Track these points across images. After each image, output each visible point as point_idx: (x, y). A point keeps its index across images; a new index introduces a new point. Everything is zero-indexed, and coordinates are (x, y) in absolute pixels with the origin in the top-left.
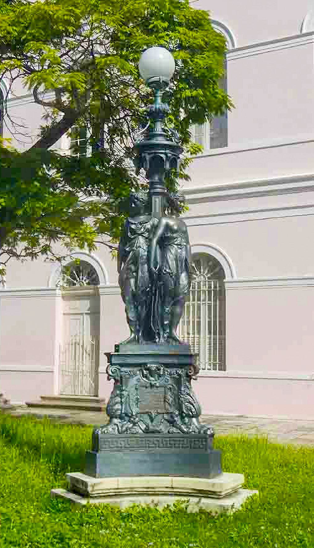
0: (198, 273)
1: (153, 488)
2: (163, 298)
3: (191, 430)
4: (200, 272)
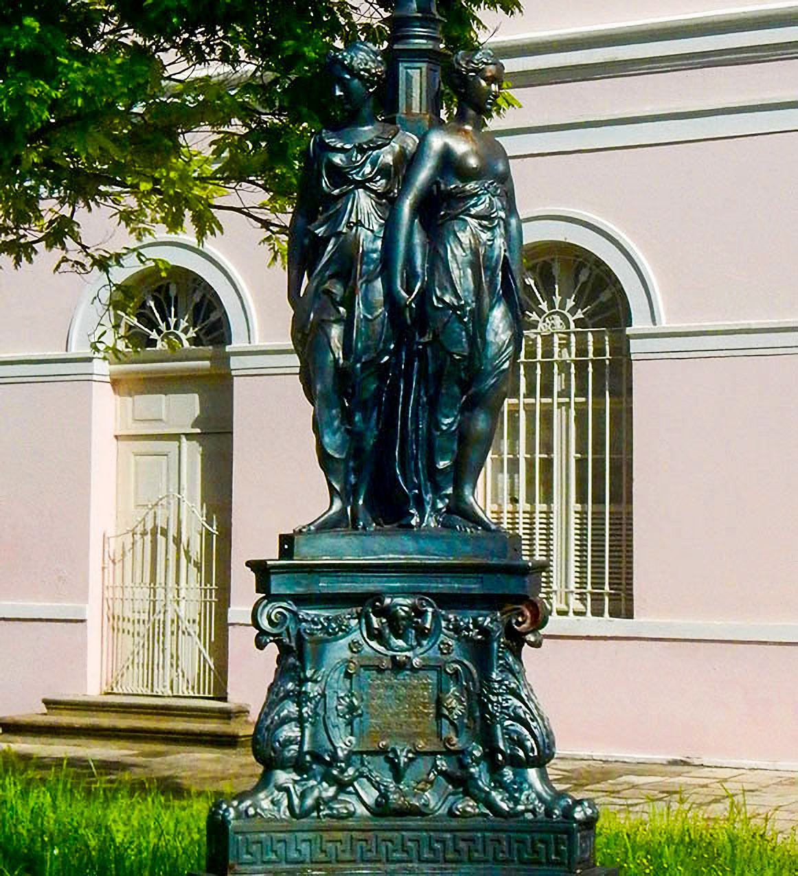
0: (544, 306)
2: (434, 383)
3: (521, 808)
4: (551, 305)
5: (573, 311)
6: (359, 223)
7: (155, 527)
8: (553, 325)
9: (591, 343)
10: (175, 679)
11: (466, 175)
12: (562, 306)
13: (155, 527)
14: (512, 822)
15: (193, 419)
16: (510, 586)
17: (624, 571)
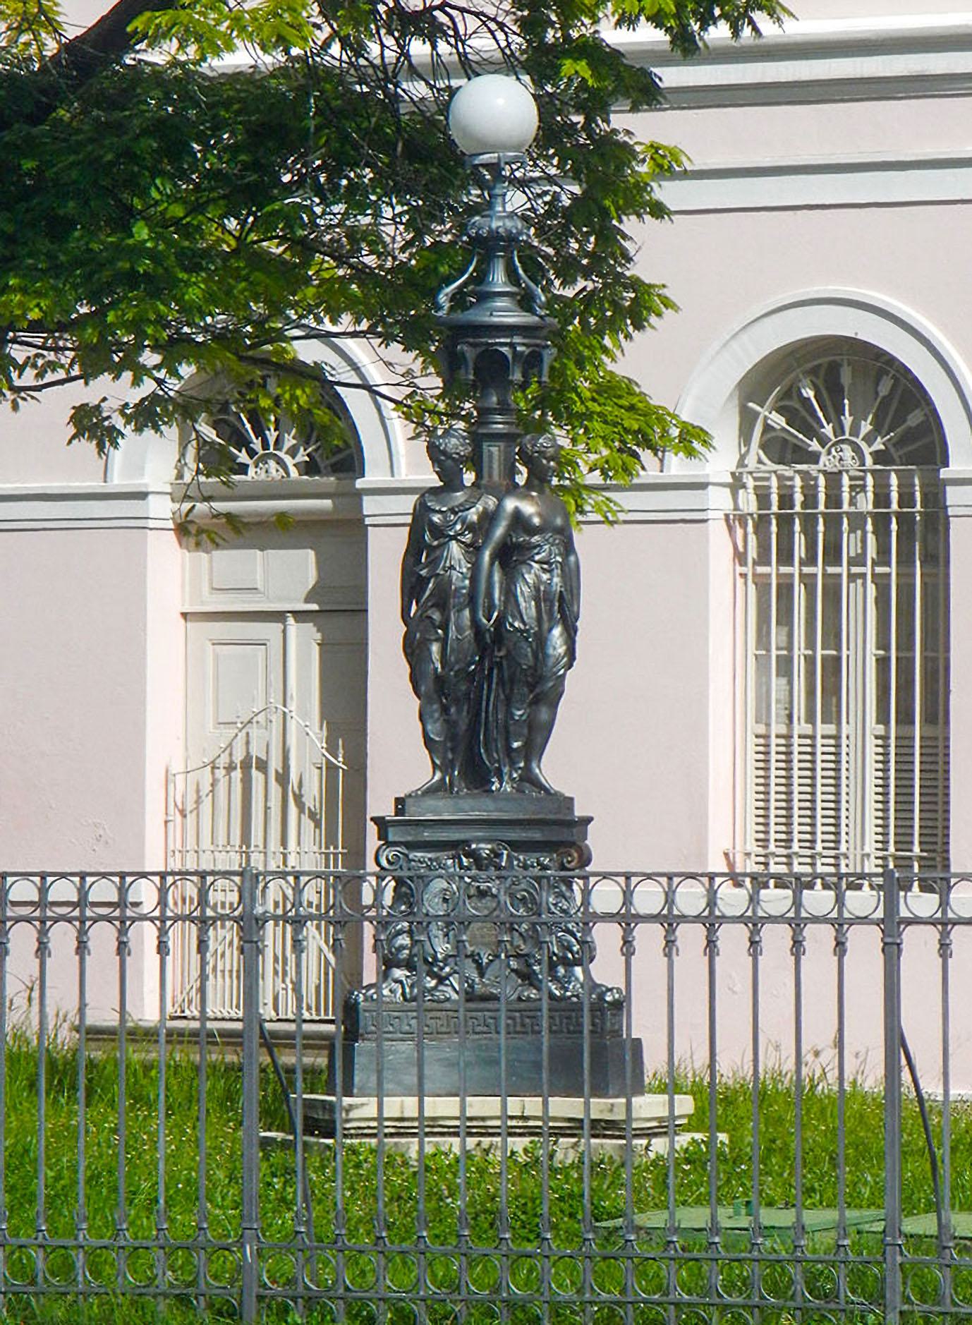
0: (828, 430)
1: (483, 1119)
2: (508, 684)
3: (569, 994)
4: (839, 430)
5: (869, 439)
6: (452, 567)
7: (248, 757)
8: (841, 459)
9: (894, 488)
10: (282, 993)
11: (533, 531)
12: (855, 430)
13: (248, 757)
14: (563, 1004)
15: (306, 592)
16: (564, 835)
17: (939, 840)
